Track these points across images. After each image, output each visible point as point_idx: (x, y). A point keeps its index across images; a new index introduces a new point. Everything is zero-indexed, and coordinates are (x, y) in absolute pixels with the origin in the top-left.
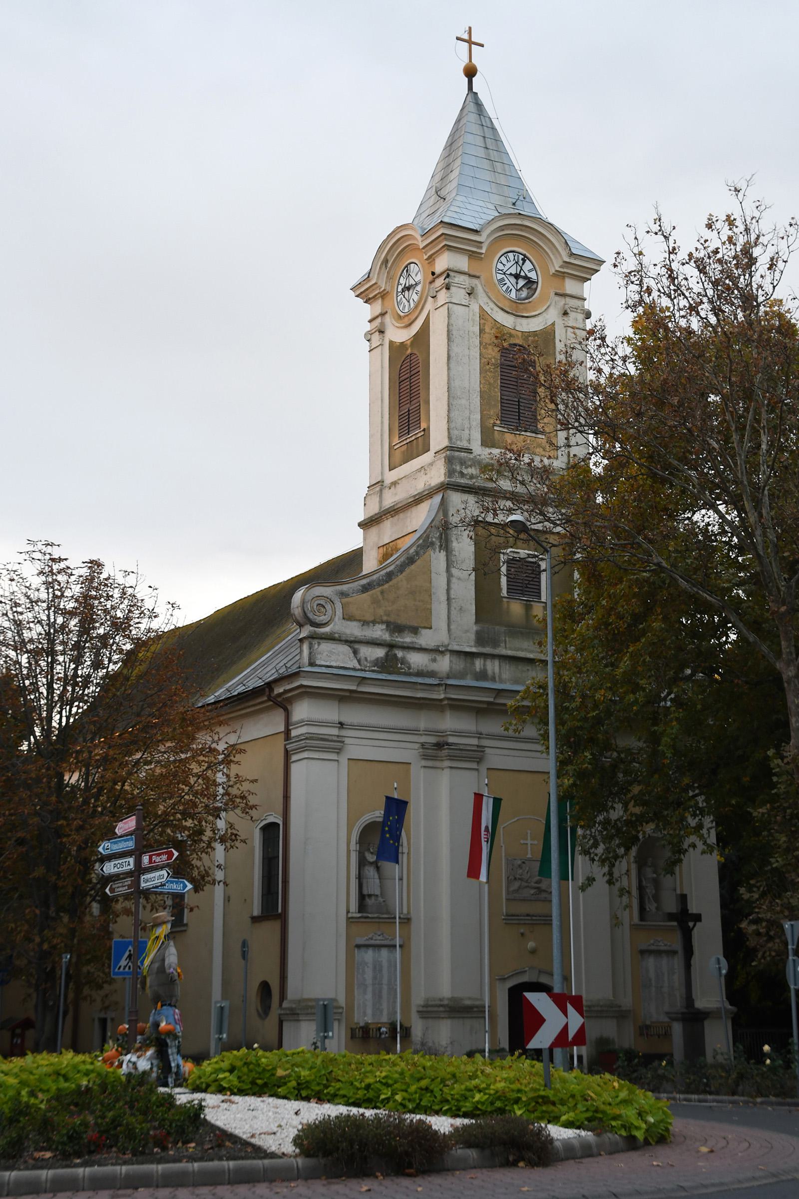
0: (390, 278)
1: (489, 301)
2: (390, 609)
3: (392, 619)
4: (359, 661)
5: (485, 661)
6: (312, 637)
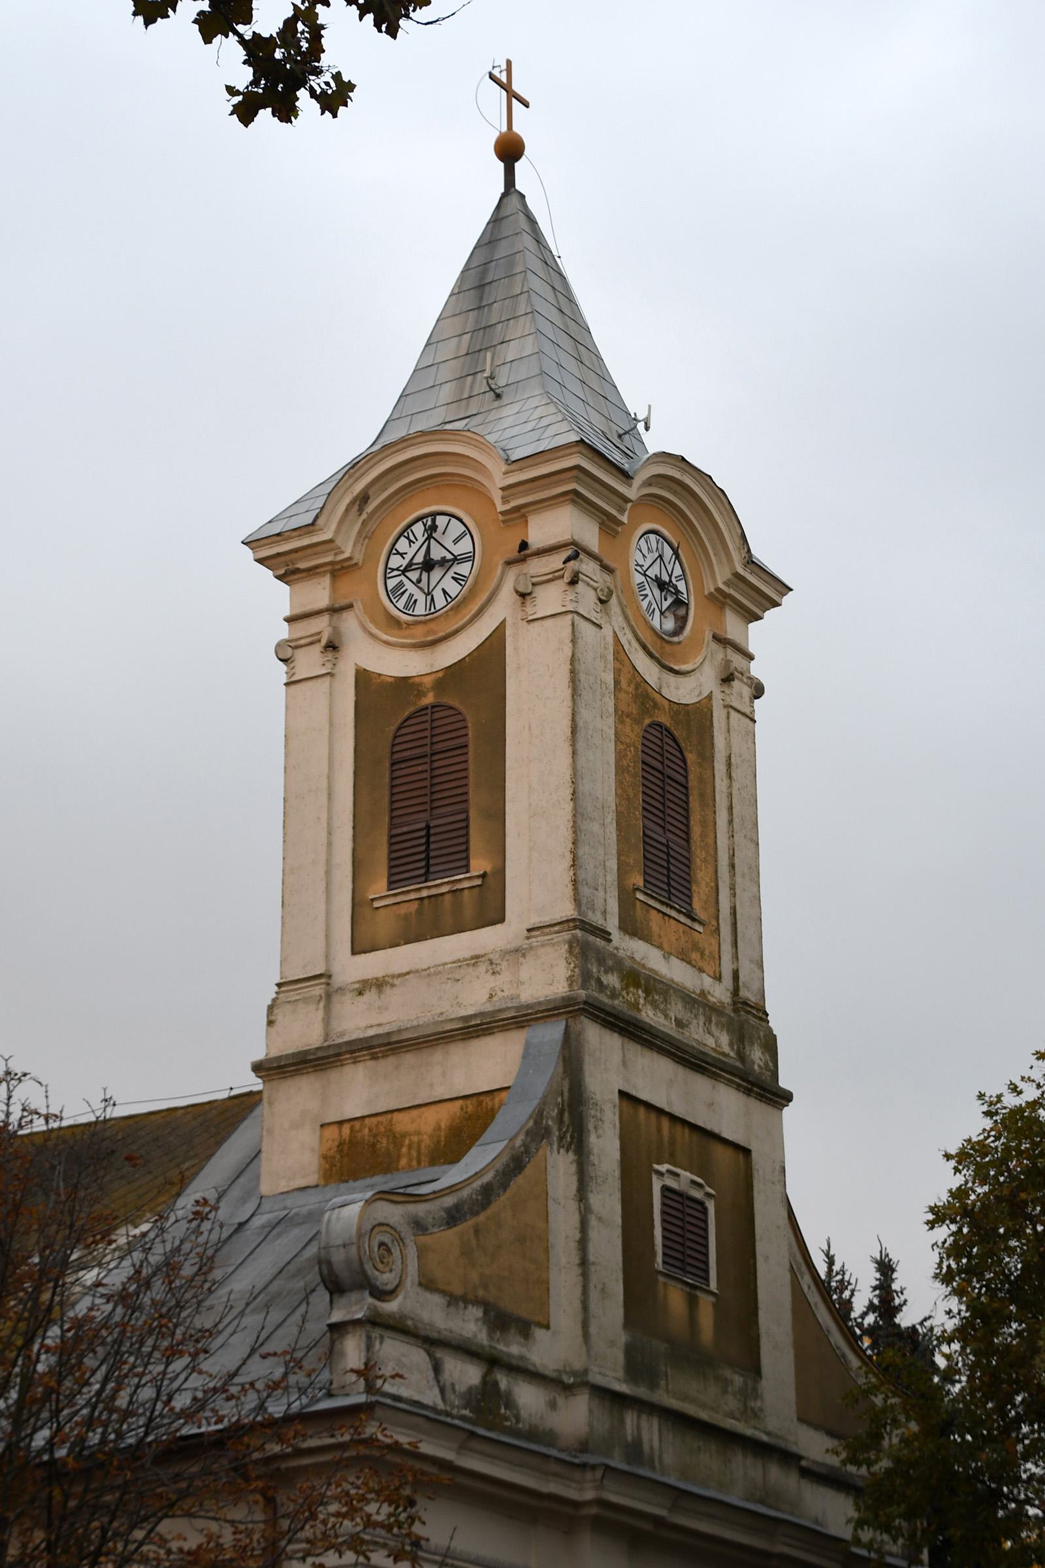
0: (366, 536)
1: (625, 625)
4: (442, 1391)
5: (639, 1417)
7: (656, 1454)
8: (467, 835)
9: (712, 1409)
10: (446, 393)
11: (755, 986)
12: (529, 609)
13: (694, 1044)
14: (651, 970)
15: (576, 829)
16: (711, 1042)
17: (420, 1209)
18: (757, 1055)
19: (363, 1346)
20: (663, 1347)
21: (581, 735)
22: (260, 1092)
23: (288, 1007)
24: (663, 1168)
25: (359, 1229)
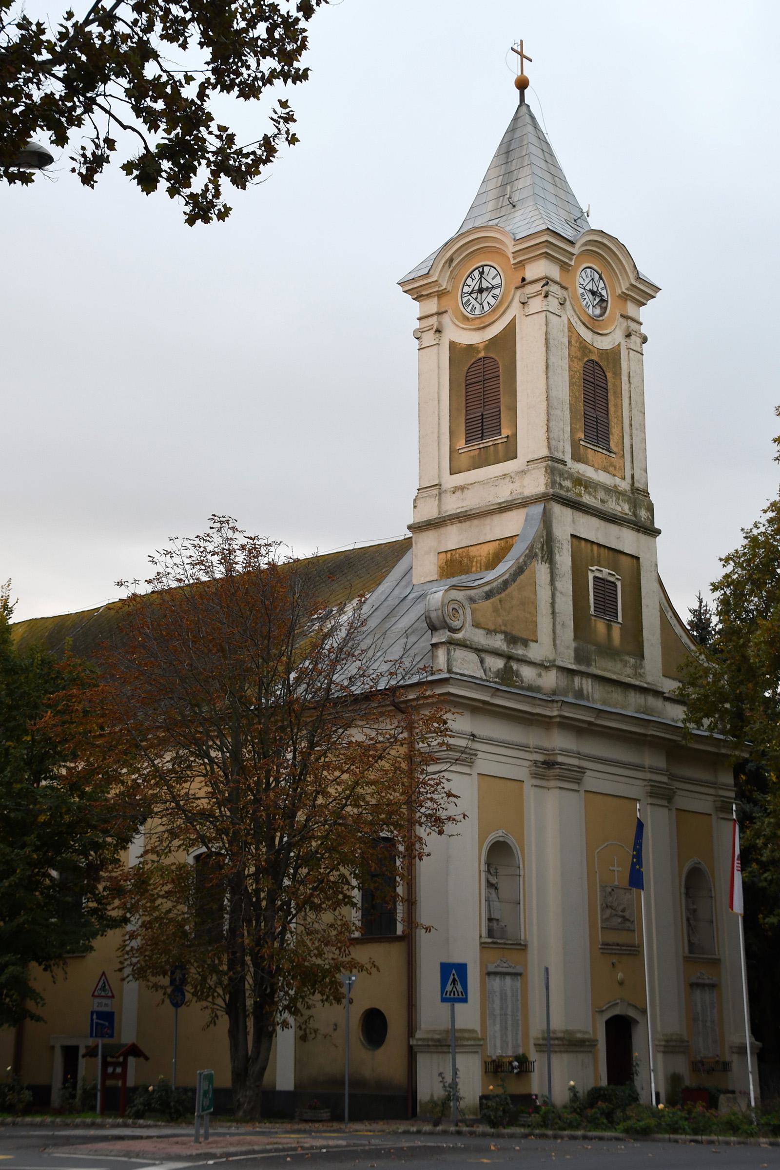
0: (453, 278)
1: (574, 314)
2: (506, 618)
3: (508, 629)
4: (485, 671)
5: (581, 679)
6: (451, 643)
7: (590, 695)
8: (500, 418)
9: (619, 674)
10: (491, 206)
11: (643, 481)
12: (526, 310)
13: (610, 511)
14: (588, 477)
15: (548, 414)
16: (619, 509)
17: (472, 593)
18: (643, 514)
19: (446, 653)
20: (593, 648)
21: (550, 369)
22: (411, 537)
23: (422, 499)
24: (594, 568)
25: (442, 602)
